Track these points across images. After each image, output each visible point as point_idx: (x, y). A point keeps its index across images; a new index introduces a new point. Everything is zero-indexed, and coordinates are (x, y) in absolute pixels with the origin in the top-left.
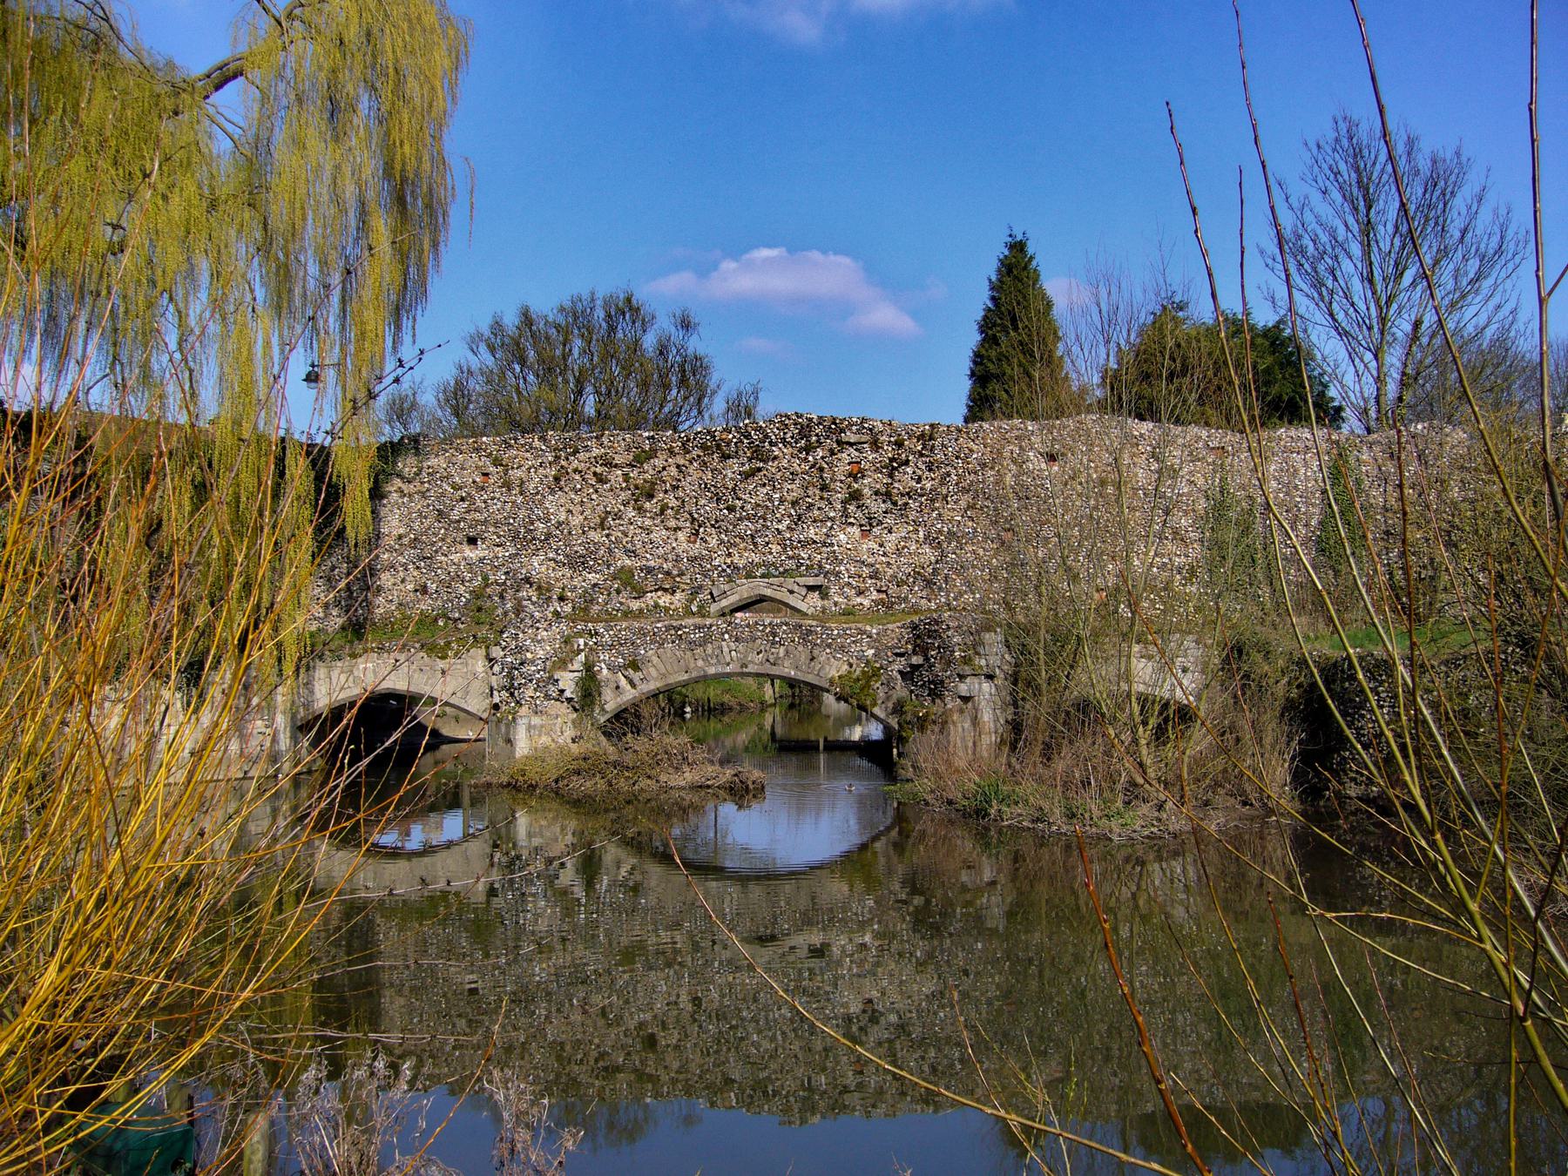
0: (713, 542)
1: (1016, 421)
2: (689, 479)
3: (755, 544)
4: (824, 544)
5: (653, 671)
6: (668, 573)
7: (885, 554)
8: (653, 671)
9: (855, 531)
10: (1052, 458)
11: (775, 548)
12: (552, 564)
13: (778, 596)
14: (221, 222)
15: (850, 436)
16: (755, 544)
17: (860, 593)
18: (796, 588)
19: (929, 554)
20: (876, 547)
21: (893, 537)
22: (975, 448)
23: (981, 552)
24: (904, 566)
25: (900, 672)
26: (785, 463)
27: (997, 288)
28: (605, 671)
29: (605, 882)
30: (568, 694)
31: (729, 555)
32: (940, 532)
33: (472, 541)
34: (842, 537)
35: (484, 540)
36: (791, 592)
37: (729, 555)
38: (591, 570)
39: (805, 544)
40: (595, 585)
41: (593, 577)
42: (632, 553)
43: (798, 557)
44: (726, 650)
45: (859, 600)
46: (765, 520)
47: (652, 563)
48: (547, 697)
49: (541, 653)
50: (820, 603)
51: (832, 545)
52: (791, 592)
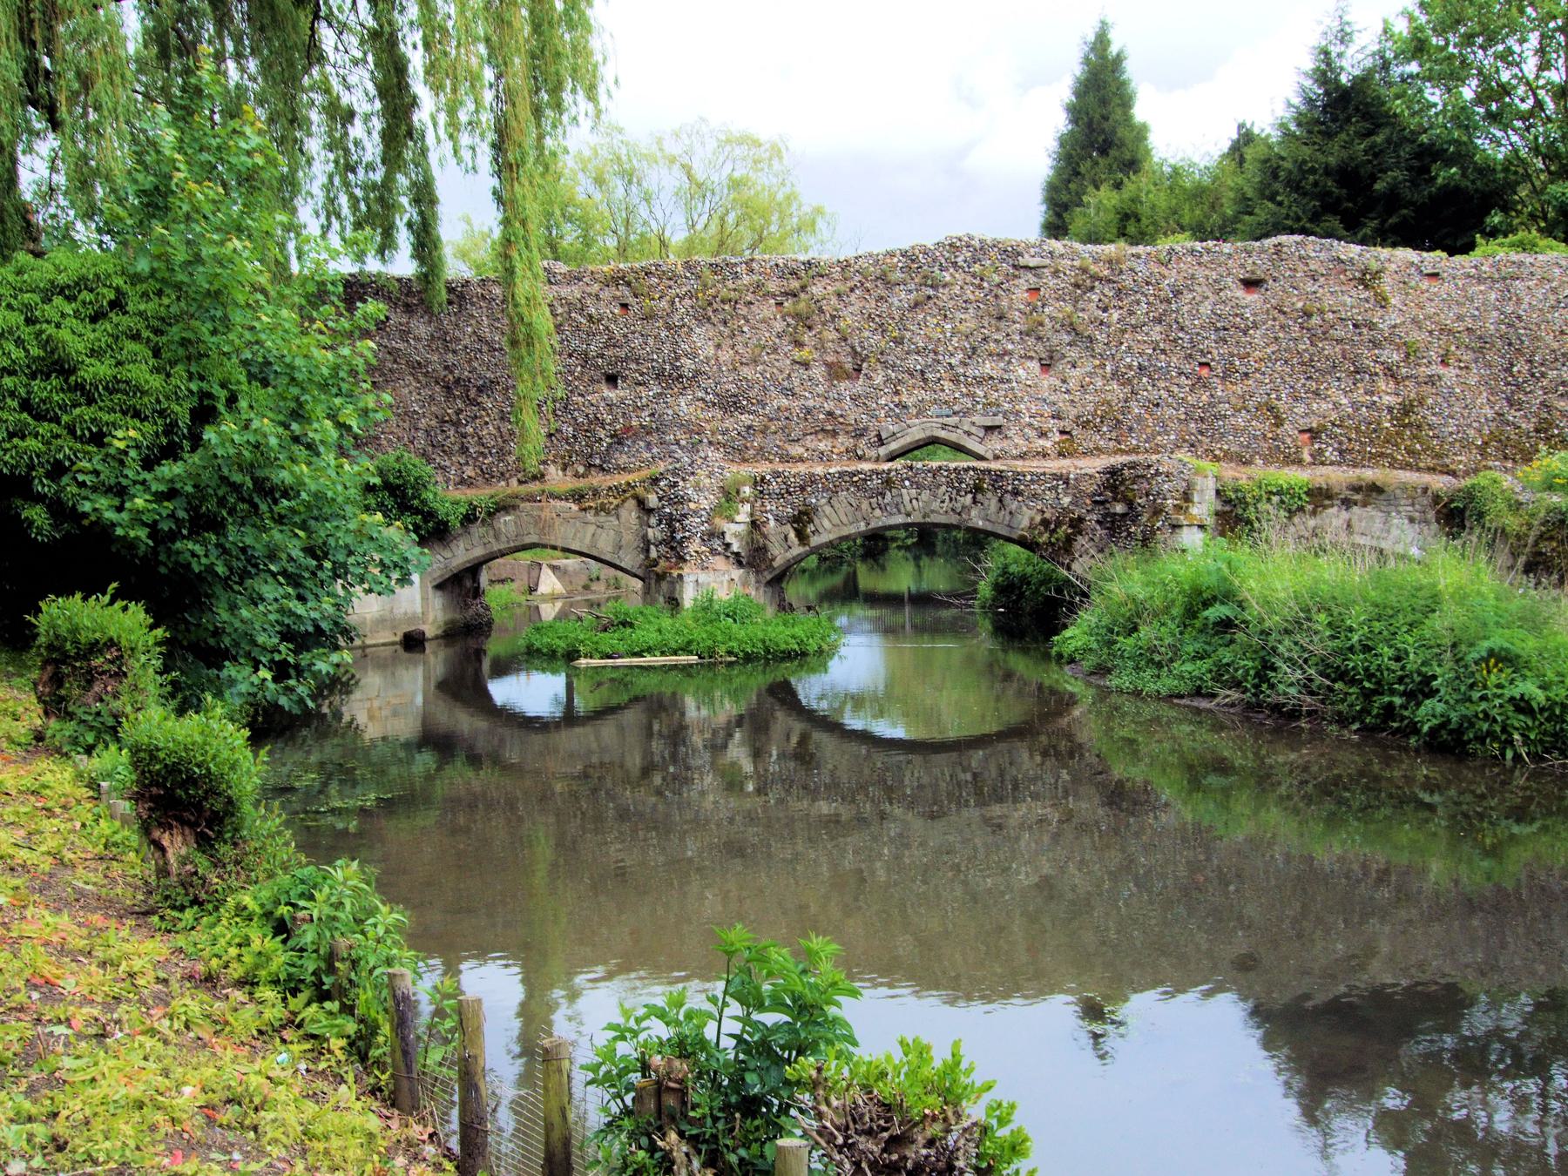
0: (879, 380)
1: (1210, 243)
2: (851, 309)
3: (925, 380)
4: (1002, 381)
5: (826, 523)
6: (830, 414)
7: (1068, 392)
8: (826, 523)
9: (1034, 366)
10: (1251, 284)
11: (947, 385)
12: (700, 404)
13: (953, 437)
14: (272, 556)
15: (1026, 260)
16: (925, 380)
17: (1043, 434)
18: (973, 430)
19: (1116, 391)
20: (1058, 383)
21: (1077, 372)
22: (1166, 272)
23: (1176, 389)
24: (1088, 404)
25: (1098, 522)
26: (957, 290)
27: (1076, 113)
28: (772, 523)
29: (774, 753)
30: (735, 548)
31: (897, 393)
32: (1130, 367)
33: (612, 380)
34: (1021, 372)
35: (625, 379)
36: (969, 434)
37: (897, 393)
38: (743, 410)
39: (980, 381)
40: (749, 427)
41: (746, 419)
42: (790, 393)
43: (973, 395)
44: (906, 498)
45: (1041, 442)
46: (936, 353)
47: (810, 403)
48: (713, 552)
49: (705, 504)
50: (79, 226)
51: (1009, 381)
52: (969, 434)
